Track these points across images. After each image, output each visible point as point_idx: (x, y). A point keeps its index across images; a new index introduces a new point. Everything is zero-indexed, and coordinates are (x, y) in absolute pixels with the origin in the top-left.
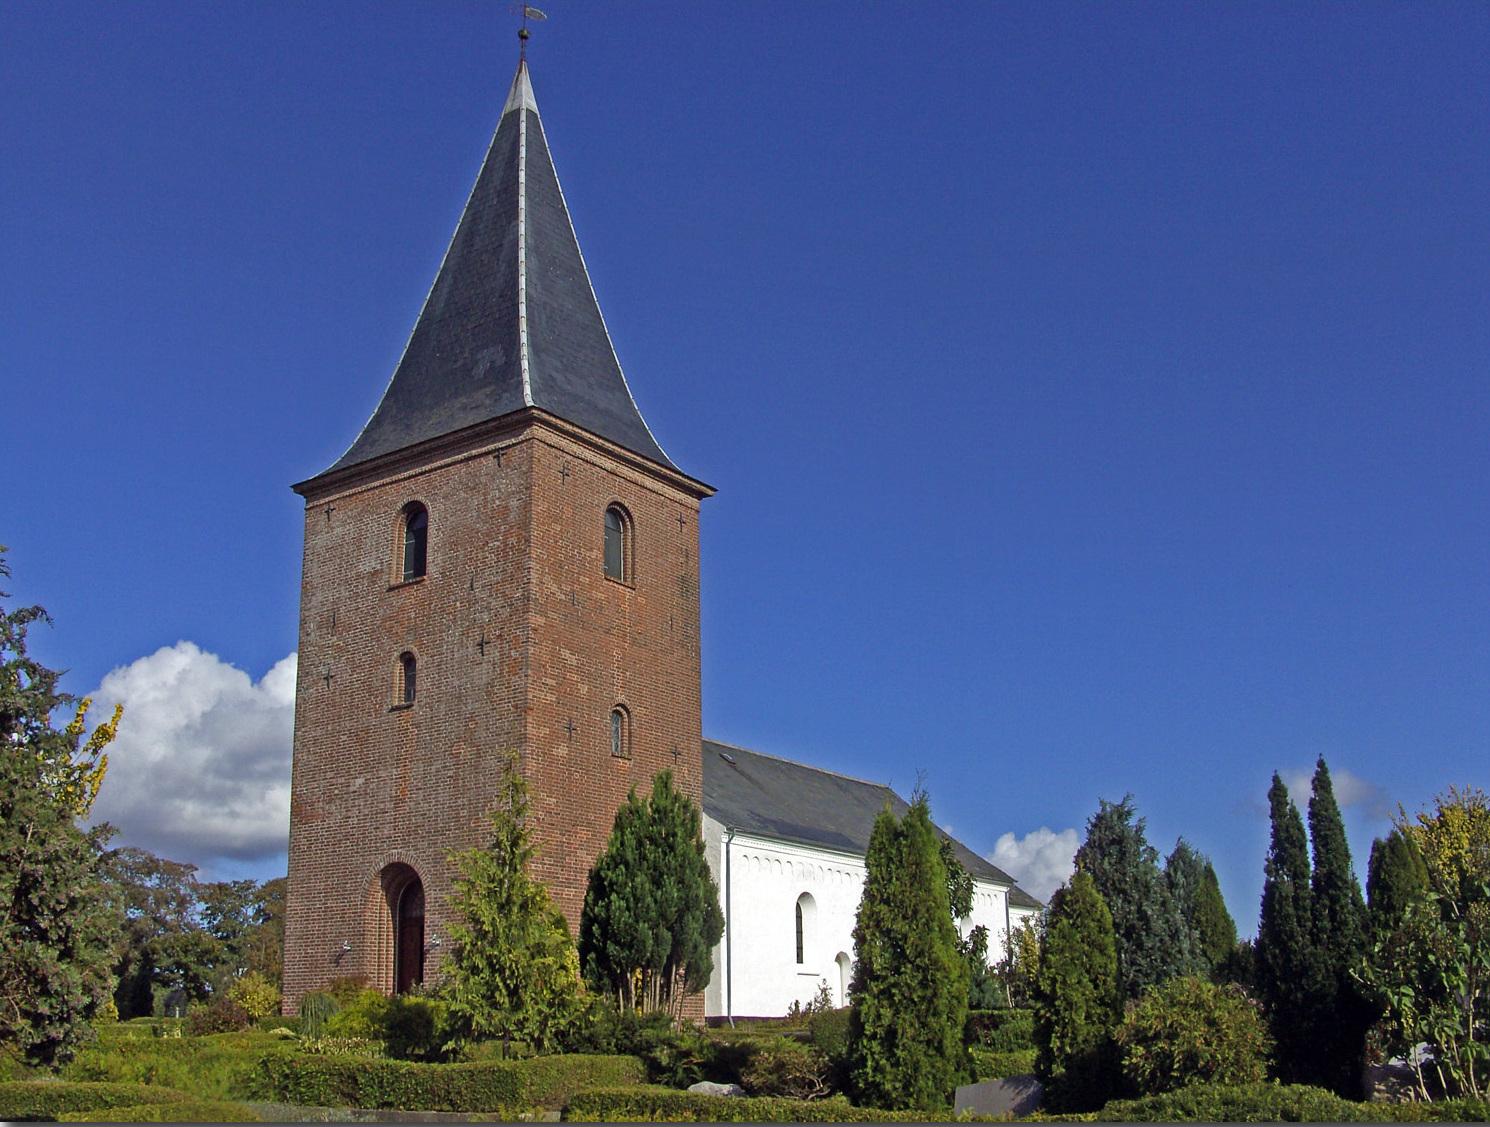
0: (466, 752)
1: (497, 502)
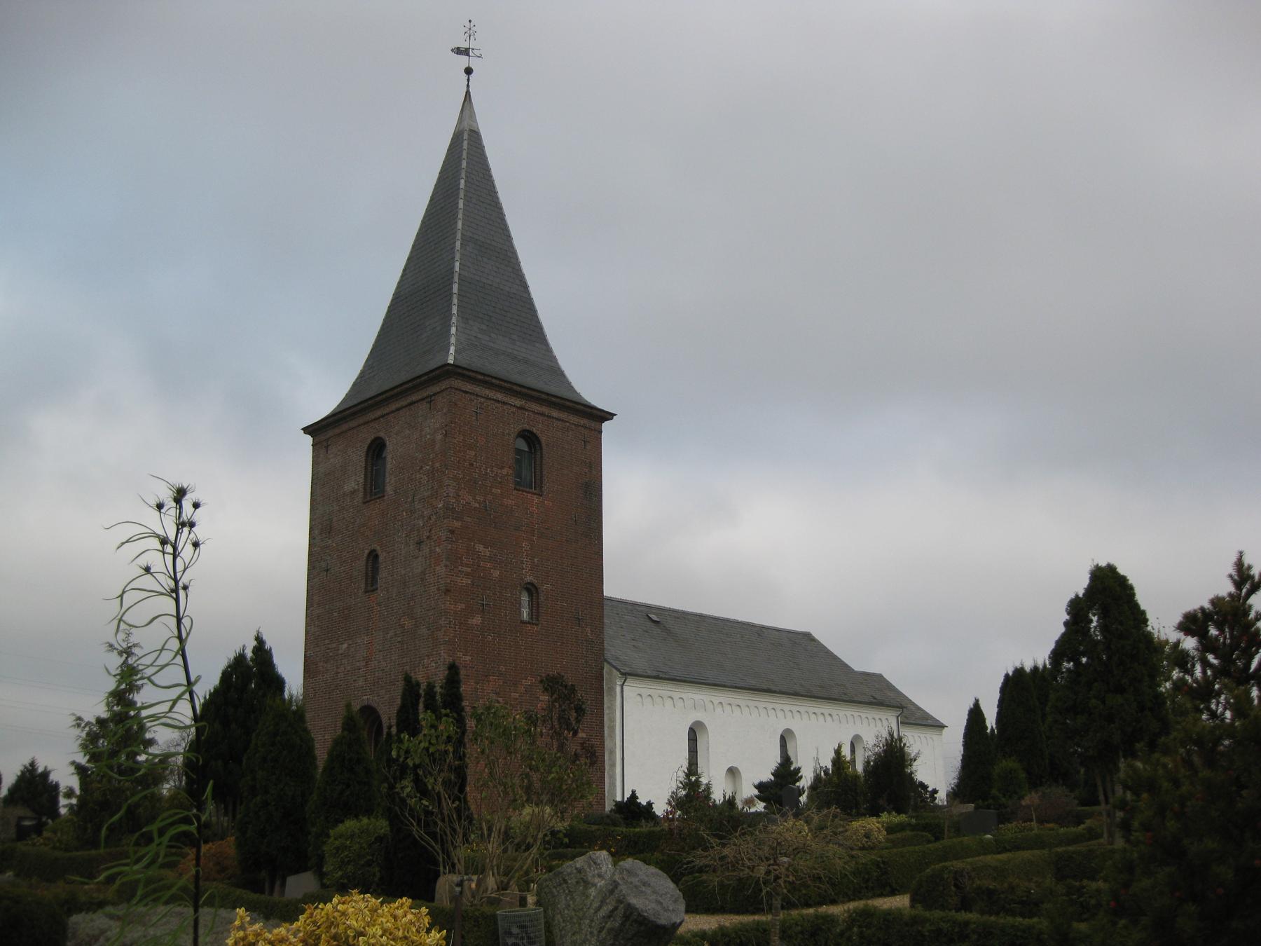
0: (408, 623)
1: (428, 437)
